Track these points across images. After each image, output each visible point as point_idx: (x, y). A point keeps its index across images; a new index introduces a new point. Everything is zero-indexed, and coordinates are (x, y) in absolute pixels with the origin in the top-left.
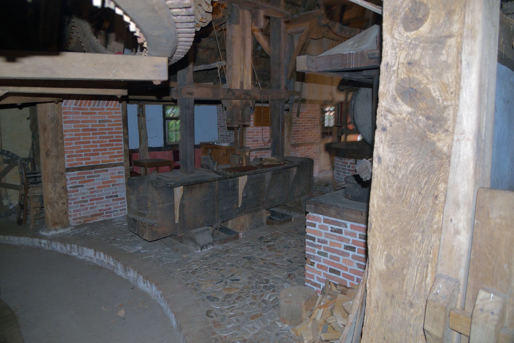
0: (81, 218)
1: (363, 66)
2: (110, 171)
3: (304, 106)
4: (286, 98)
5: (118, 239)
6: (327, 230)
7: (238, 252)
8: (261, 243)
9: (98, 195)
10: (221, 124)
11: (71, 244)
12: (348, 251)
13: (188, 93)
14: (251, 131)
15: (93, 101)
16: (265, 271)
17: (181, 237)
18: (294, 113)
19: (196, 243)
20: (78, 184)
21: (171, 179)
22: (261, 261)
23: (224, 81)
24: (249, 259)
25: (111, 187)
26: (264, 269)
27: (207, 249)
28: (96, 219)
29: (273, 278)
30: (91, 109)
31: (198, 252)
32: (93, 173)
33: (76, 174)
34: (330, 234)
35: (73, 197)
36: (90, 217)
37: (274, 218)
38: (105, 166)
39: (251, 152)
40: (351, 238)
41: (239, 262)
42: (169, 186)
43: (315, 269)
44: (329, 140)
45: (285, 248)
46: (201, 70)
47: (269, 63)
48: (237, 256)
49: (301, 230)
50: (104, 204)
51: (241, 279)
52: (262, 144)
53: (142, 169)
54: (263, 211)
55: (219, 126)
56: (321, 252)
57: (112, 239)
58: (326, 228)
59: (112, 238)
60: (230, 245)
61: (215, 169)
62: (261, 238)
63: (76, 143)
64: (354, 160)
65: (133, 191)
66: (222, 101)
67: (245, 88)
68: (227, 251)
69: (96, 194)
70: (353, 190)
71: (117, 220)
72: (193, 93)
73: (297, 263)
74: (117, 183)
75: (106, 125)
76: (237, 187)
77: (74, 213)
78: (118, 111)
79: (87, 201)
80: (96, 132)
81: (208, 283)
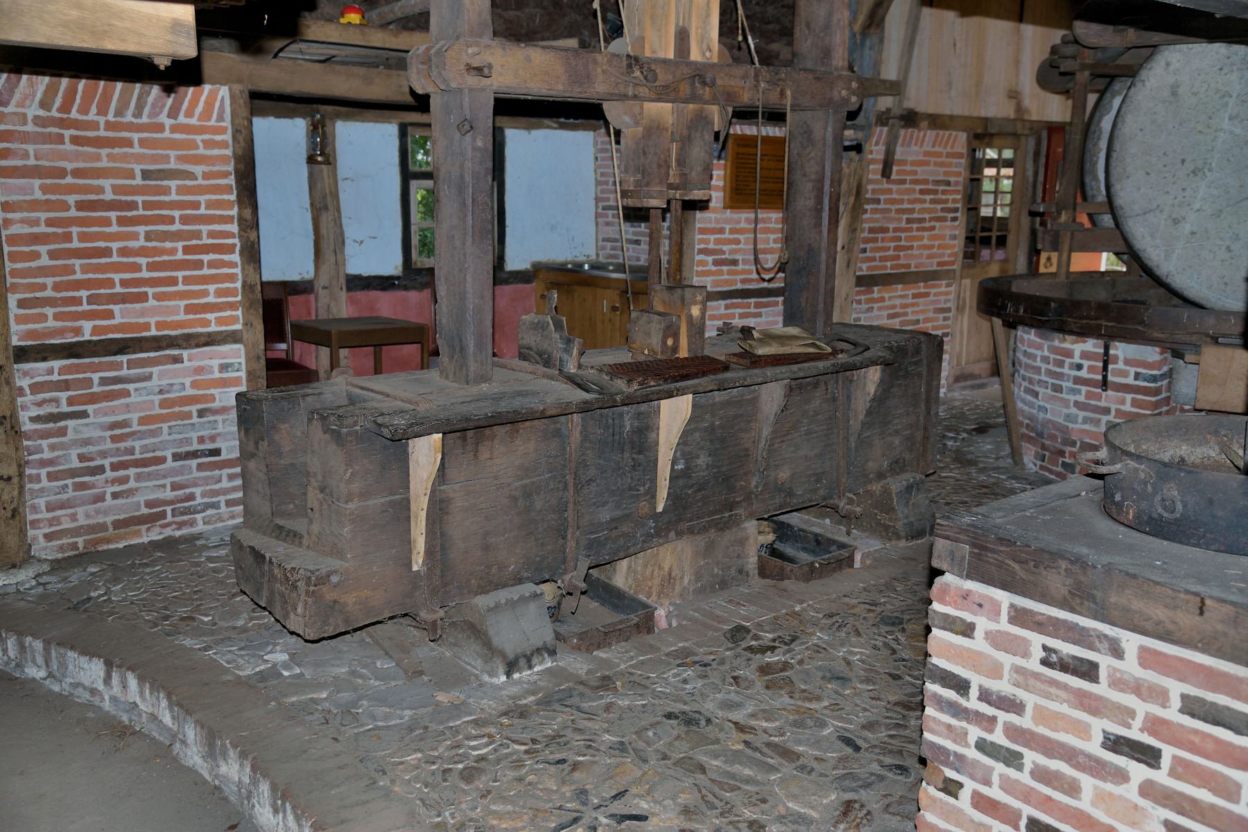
0: (76, 532)
2: (190, 360)
3: (911, 137)
4: (854, 99)
5: (206, 619)
6: (1026, 655)
7: (646, 688)
9: (145, 449)
11: (21, 634)
12: (1120, 761)
14: (713, 225)
16: (748, 781)
17: (434, 623)
18: (873, 161)
19: (490, 650)
20: (65, 408)
22: (735, 734)
23: (616, 30)
24: (689, 721)
25: (195, 420)
26: (747, 772)
27: (529, 672)
28: (138, 534)
29: (781, 819)
30: (110, 126)
31: (495, 680)
32: (125, 366)
33: (56, 371)
34: (1037, 676)
35: (47, 455)
36: (111, 529)
38: (172, 342)
39: (708, 303)
40: (1143, 708)
41: (650, 734)
42: (385, 432)
43: (960, 811)
44: (992, 263)
48: (644, 706)
49: (889, 607)
50: (168, 481)
51: (653, 814)
52: (750, 272)
53: (324, 352)
54: (747, 525)
55: (601, 204)
56: (992, 743)
57: (183, 619)
58: (1020, 648)
59: (183, 611)
60: (617, 656)
61: (572, 368)
62: (738, 633)
63: (53, 255)
64: (1101, 342)
65: (257, 443)
66: (606, 106)
67: (695, 55)
68: (606, 683)
69: (137, 444)
70: (1150, 488)
71: (215, 540)
72: (490, 67)
73: (877, 751)
76: (653, 435)
77: (50, 515)
78: (218, 138)
79: (100, 470)
80: (134, 213)
81: (520, 824)
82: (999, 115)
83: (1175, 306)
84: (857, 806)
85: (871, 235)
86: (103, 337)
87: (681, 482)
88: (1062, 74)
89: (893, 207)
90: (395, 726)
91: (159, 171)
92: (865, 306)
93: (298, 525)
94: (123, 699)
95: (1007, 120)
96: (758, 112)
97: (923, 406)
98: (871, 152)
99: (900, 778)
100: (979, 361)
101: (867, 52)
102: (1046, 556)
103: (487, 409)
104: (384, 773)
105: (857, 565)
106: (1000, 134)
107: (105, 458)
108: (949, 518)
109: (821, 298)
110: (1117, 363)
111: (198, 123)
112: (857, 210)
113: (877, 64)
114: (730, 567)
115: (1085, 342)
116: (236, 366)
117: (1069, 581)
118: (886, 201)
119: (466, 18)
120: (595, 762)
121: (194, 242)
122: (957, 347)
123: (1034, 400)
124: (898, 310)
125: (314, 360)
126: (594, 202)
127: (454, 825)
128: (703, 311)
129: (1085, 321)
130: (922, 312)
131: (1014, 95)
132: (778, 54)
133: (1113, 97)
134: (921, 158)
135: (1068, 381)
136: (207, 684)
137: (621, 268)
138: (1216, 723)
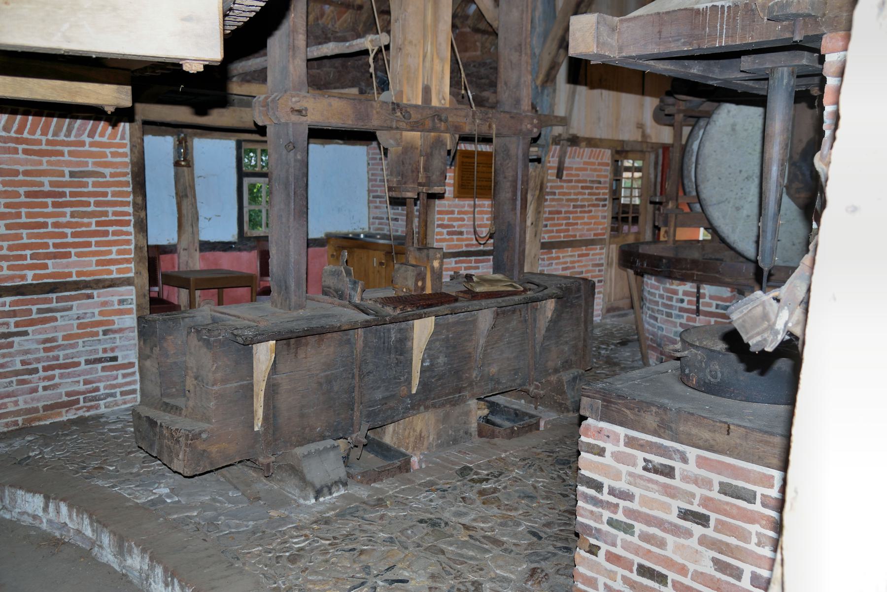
1: (750, 41)
2: (98, 297)
3: (575, 152)
4: (535, 130)
5: (111, 468)
6: (634, 465)
7: (406, 504)
8: (464, 485)
9: (66, 357)
10: (377, 191)
12: (688, 524)
13: (293, 110)
14: (447, 209)
15: (55, 120)
16: (472, 558)
17: (268, 465)
18: (551, 168)
20: (13, 329)
21: (247, 322)
22: (463, 531)
23: (384, 85)
24: (434, 524)
25: (101, 337)
26: (471, 553)
27: (330, 497)
28: (60, 414)
29: (492, 580)
30: (49, 143)
31: (308, 503)
32: (55, 300)
33: (8, 304)
34: (641, 477)
36: (41, 412)
37: (497, 420)
38: (87, 285)
39: (445, 260)
40: (699, 492)
41: (409, 532)
42: (239, 339)
43: (599, 564)
44: (630, 233)
45: (523, 498)
46: (329, 55)
47: (493, 47)
48: (405, 516)
49: (561, 454)
50: (81, 379)
51: (412, 579)
52: (471, 239)
53: (184, 293)
54: (470, 402)
55: (371, 194)
57: (95, 468)
59: (95, 464)
60: (388, 487)
61: (357, 300)
62: (464, 471)
64: (695, 285)
65: (152, 349)
66: (378, 133)
67: (435, 103)
68: (380, 503)
69: (61, 354)
71: (113, 418)
72: (306, 109)
73: (552, 539)
74: (116, 327)
75: (90, 185)
76: (409, 343)
78: (121, 150)
79: (36, 371)
80: (64, 199)
81: (327, 587)
82: (632, 139)
83: (742, 262)
84: (539, 571)
85: (550, 216)
86: (40, 282)
87: (427, 374)
88: (667, 115)
89: (564, 198)
90: (243, 531)
91: (81, 172)
92: (547, 262)
93: (180, 402)
94: (56, 521)
95: (636, 142)
96: (474, 138)
97: (582, 325)
98: (549, 162)
99: (566, 554)
100: (623, 298)
101: (545, 97)
102: (644, 404)
103: (304, 325)
104: (238, 559)
105: (542, 428)
106: (632, 151)
107: (39, 362)
108: (589, 385)
109: (516, 256)
110: (705, 298)
111: (108, 141)
112: (540, 199)
113: (552, 106)
114: (459, 430)
115: (685, 285)
116: (130, 300)
117: (658, 419)
118: (560, 194)
119: (291, 79)
120: (374, 550)
121: (103, 218)
122: (608, 290)
123: (655, 323)
124: (569, 265)
125: (176, 298)
126: (367, 193)
127: (285, 589)
128: (441, 264)
129: (684, 271)
130: (585, 266)
131: (641, 126)
132: (488, 99)
133: (699, 129)
134: (582, 166)
135: (676, 310)
136: (116, 508)
137: (384, 237)
138: (738, 497)
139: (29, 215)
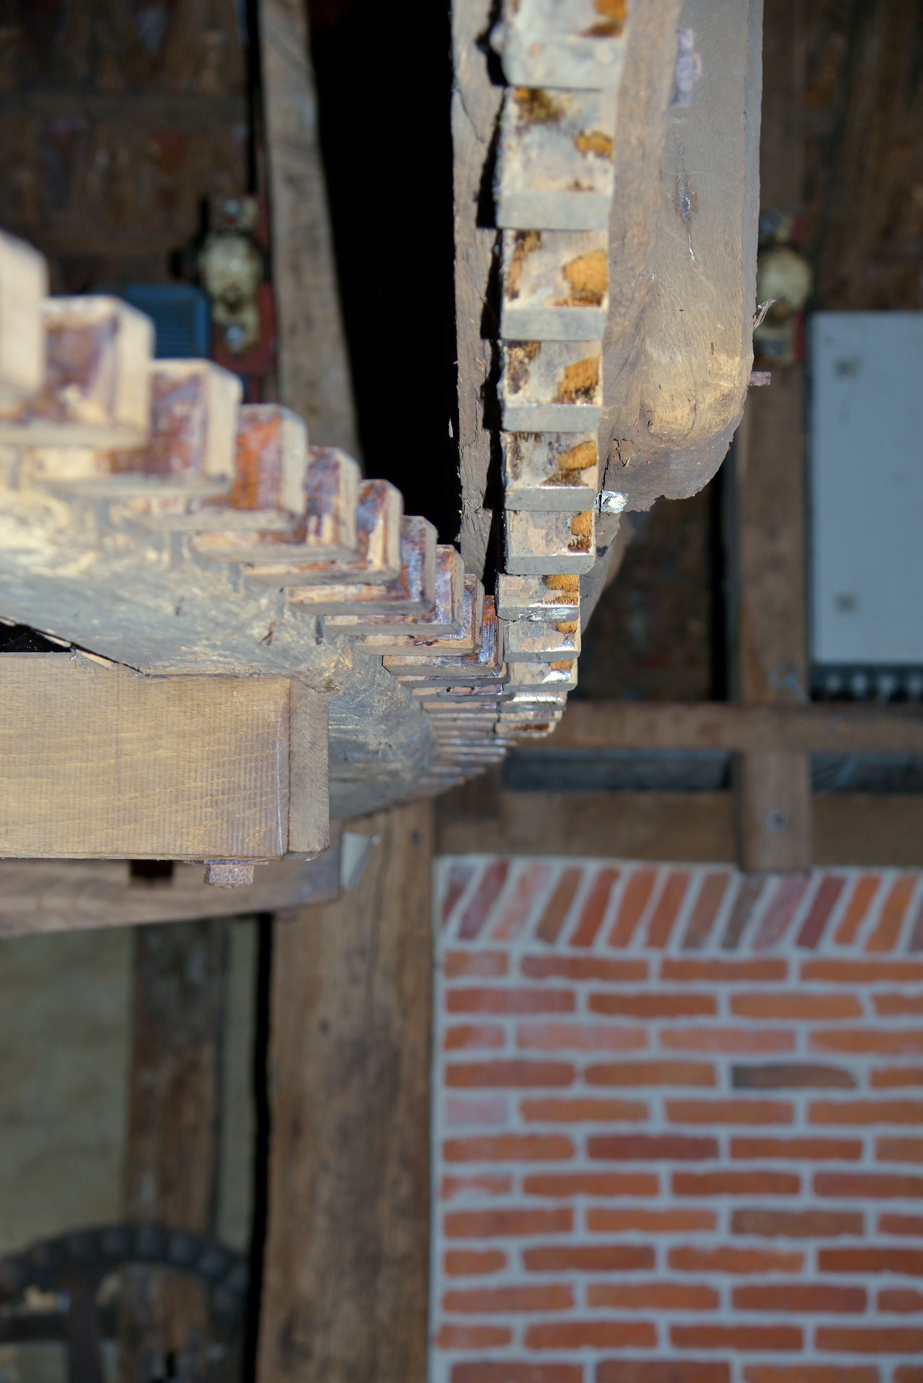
30: (671, 970)
139: (598, 1221)
